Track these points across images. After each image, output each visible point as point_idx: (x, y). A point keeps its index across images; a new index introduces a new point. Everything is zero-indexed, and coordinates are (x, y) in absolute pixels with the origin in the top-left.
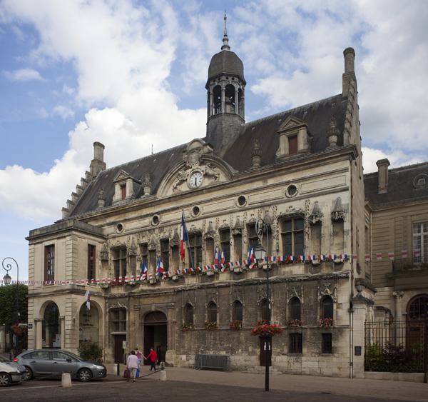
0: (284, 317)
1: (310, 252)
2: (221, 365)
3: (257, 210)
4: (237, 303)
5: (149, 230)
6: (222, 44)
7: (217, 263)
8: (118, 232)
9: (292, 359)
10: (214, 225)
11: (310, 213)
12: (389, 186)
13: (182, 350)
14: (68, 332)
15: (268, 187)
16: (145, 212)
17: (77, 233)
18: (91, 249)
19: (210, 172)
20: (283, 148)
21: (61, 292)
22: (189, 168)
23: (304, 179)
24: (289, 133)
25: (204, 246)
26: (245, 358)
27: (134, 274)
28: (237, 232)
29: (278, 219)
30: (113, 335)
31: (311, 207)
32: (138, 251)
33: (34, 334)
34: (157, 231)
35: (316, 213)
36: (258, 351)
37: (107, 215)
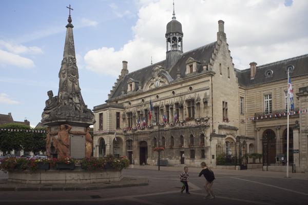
0: (188, 143)
1: (196, 116)
2: (165, 164)
4: (172, 137)
6: (172, 16)
7: (165, 120)
10: (163, 104)
12: (256, 76)
18: (118, 114)
19: (162, 80)
20: (188, 71)
21: (105, 134)
23: (195, 84)
24: (190, 64)
25: (160, 113)
26: (175, 161)
28: (171, 107)
32: (137, 114)
33: (301, 162)
34: (143, 106)
35: (199, 99)
36: (180, 158)
37: (125, 98)
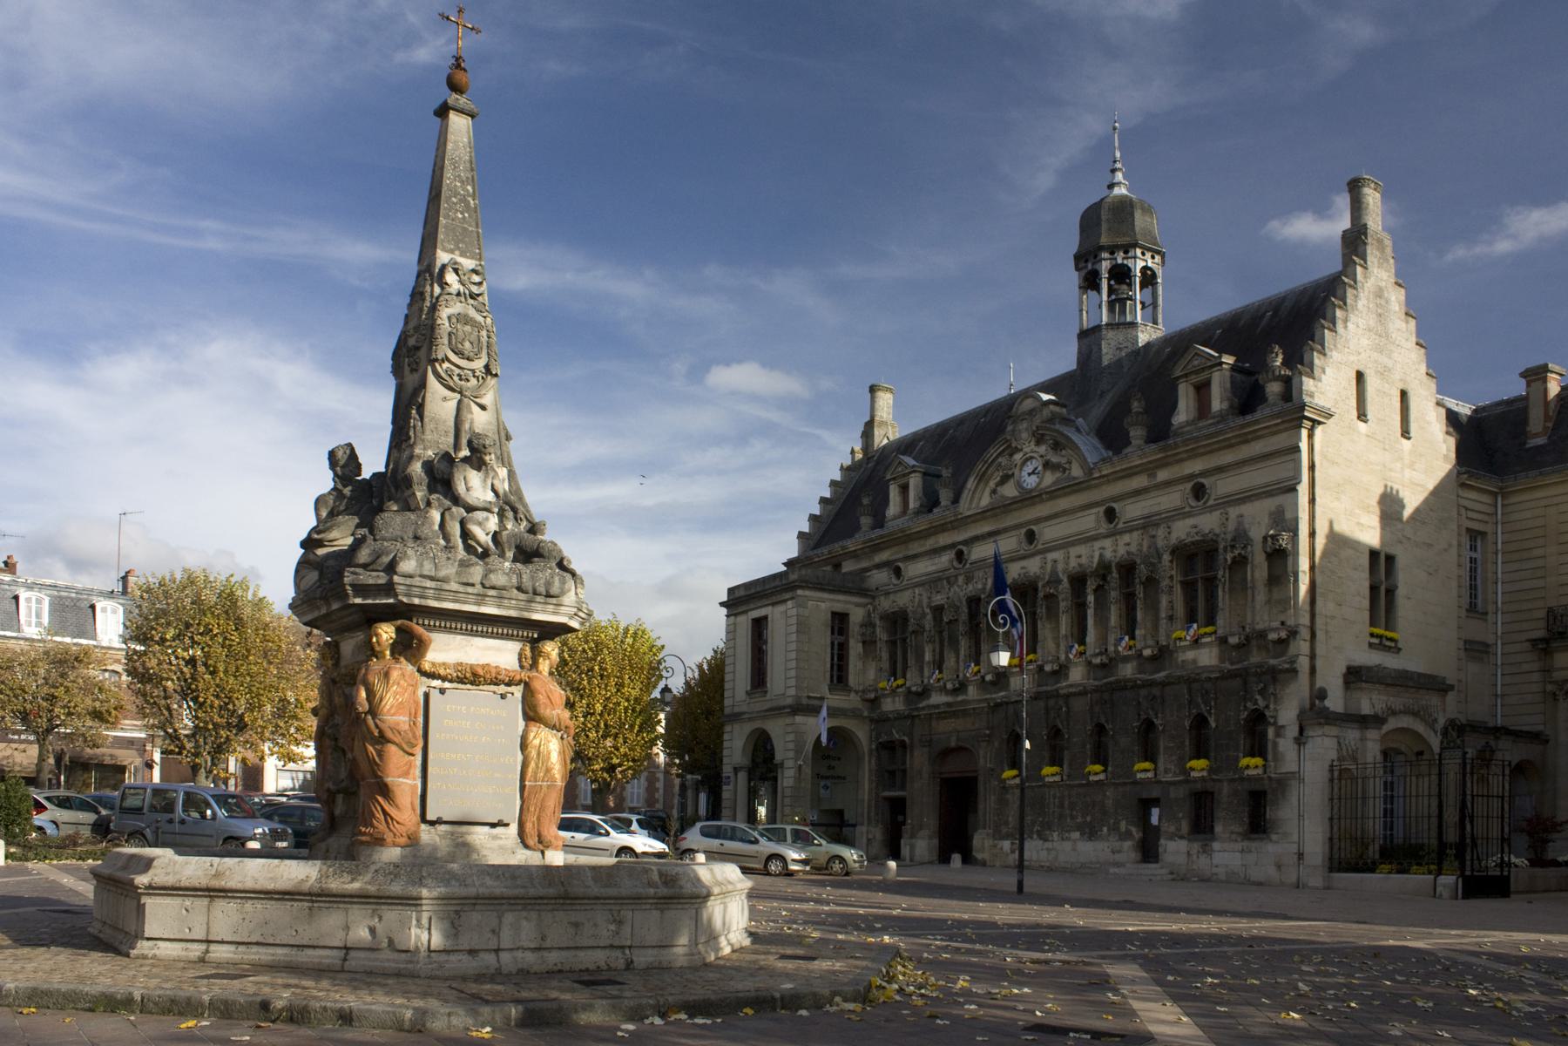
3: (1135, 534)
4: (1100, 729)
5: (948, 579)
8: (895, 581)
9: (1196, 846)
11: (1229, 537)
13: (1004, 830)
14: (788, 792)
15: (1158, 486)
16: (944, 539)
17: (807, 593)
21: (776, 711)
22: (1017, 450)
23: (1220, 470)
24: (1195, 379)
27: (921, 670)
29: (1173, 552)
30: (886, 798)
31: (1231, 526)
35: (1241, 537)
37: (876, 548)
